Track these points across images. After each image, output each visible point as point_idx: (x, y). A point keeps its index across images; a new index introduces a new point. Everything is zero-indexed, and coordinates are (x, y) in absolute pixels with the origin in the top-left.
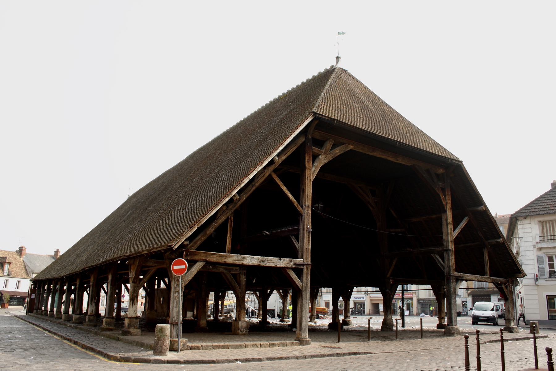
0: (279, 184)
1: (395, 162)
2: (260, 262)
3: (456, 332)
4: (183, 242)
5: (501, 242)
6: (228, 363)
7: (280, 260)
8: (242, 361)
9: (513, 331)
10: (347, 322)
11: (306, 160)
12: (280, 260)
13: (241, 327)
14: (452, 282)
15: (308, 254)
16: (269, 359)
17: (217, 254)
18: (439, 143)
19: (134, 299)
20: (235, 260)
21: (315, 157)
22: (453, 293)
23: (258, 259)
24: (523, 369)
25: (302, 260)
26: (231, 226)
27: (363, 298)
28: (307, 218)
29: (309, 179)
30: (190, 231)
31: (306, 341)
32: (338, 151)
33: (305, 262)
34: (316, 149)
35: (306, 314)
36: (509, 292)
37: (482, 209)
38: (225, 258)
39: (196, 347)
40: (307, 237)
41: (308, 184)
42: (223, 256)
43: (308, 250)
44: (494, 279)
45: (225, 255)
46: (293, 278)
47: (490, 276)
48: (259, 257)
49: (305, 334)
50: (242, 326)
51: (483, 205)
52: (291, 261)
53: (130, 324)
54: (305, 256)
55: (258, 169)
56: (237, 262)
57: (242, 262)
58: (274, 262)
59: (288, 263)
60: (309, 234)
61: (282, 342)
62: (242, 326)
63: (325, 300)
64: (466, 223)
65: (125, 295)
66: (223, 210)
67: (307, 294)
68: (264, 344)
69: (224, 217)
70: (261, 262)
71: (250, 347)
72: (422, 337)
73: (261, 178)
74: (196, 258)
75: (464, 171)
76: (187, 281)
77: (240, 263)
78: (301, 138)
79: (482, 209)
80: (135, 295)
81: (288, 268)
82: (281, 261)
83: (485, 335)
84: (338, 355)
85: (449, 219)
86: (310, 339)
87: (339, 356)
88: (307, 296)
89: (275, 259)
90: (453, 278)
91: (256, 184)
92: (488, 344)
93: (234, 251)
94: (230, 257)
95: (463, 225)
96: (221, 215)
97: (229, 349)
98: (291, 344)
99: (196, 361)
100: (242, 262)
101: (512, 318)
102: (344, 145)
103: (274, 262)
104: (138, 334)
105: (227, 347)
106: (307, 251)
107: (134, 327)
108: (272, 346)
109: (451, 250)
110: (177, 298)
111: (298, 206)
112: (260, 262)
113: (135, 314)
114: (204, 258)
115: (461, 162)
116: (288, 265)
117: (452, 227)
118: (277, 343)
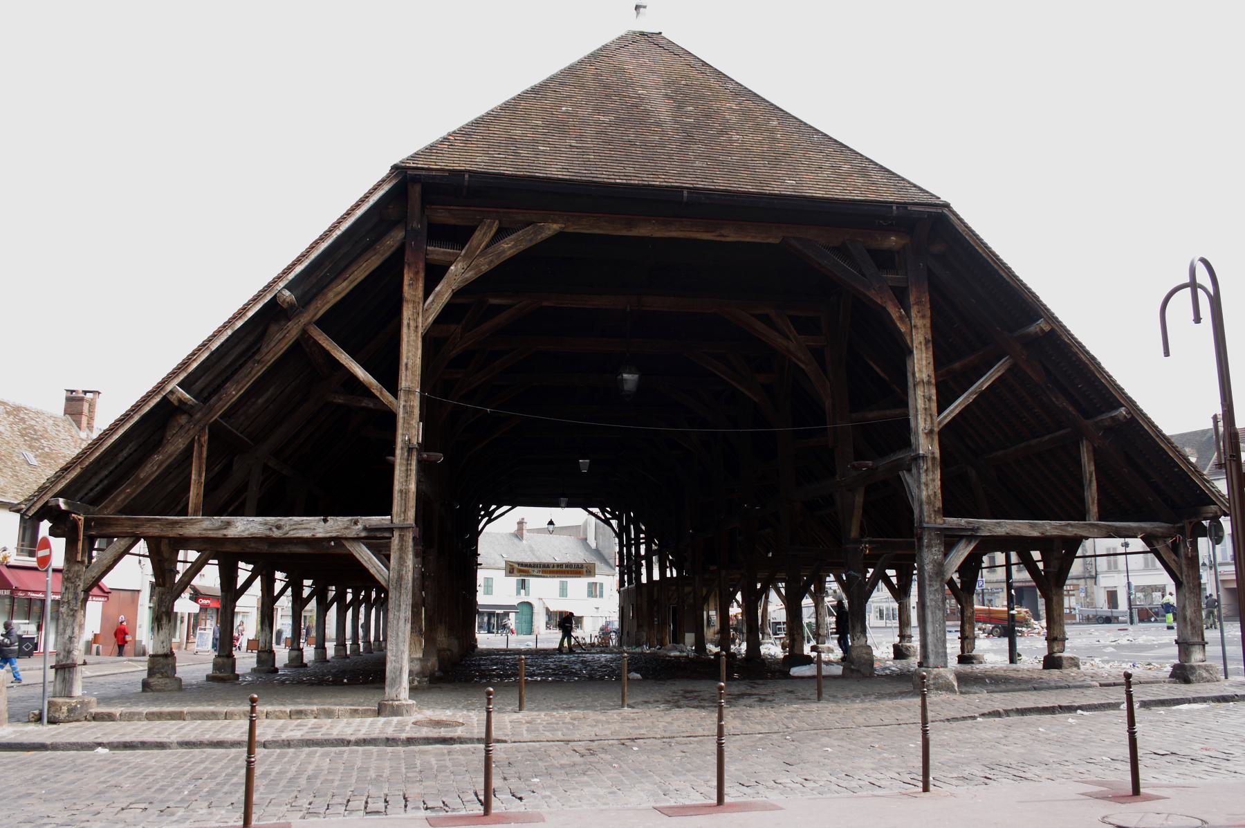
0: (328, 348)
1: (716, 241)
2: (270, 529)
3: (934, 684)
4: (47, 502)
5: (1121, 418)
6: (77, 750)
7: (325, 521)
8: (113, 746)
9: (1191, 678)
10: (902, 650)
11: (406, 282)
12: (325, 521)
14: (930, 546)
15: (405, 504)
16: (186, 745)
17: (162, 519)
18: (884, 166)
19: (162, 619)
20: (205, 530)
21: (434, 274)
22: (930, 576)
23: (266, 524)
24: (225, 825)
25: (389, 517)
26: (200, 457)
28: (404, 418)
29: (412, 324)
30: (64, 477)
31: (392, 706)
32: (508, 247)
33: (394, 521)
34: (437, 252)
35: (397, 645)
36: (1184, 561)
37: (1038, 329)
38: (181, 527)
39: (107, 715)
40: (405, 462)
41: (409, 337)
42: (176, 522)
43: (406, 494)
44: (1117, 527)
45: (180, 520)
46: (361, 560)
47: (1100, 520)
48: (268, 518)
49: (394, 690)
51: (1041, 317)
52: (356, 523)
53: (153, 668)
54: (396, 508)
55: (233, 326)
56: (212, 534)
57: (225, 532)
58: (308, 526)
59: (346, 528)
60: (408, 455)
61: (326, 707)
63: (1105, 587)
64: (999, 374)
66: (178, 424)
67: (400, 596)
68: (275, 711)
69: (180, 440)
70: (274, 529)
71: (237, 717)
72: (819, 698)
73: (277, 343)
74: (112, 531)
75: (960, 228)
76: (90, 579)
77: (220, 534)
78: (392, 234)
79: (1038, 329)
80: (164, 610)
81: (346, 539)
82: (328, 524)
83: (1066, 690)
84: (390, 742)
85: (920, 371)
86: (414, 702)
87: (394, 744)
88: (400, 601)
89: (311, 520)
90: (933, 534)
91: (265, 358)
92: (980, 723)
93: (211, 509)
94: (192, 523)
95: (983, 383)
96: (174, 435)
97: (184, 720)
98: (351, 713)
99: (8, 743)
100: (225, 532)
101: (1196, 640)
103: (307, 528)
104: (166, 689)
105: (214, 716)
106: (404, 495)
107: (162, 674)
108: (298, 717)
109: (924, 457)
110: (65, 615)
112: (270, 529)
114: (130, 531)
115: (947, 206)
116: (348, 531)
117: (934, 391)
118: (312, 711)
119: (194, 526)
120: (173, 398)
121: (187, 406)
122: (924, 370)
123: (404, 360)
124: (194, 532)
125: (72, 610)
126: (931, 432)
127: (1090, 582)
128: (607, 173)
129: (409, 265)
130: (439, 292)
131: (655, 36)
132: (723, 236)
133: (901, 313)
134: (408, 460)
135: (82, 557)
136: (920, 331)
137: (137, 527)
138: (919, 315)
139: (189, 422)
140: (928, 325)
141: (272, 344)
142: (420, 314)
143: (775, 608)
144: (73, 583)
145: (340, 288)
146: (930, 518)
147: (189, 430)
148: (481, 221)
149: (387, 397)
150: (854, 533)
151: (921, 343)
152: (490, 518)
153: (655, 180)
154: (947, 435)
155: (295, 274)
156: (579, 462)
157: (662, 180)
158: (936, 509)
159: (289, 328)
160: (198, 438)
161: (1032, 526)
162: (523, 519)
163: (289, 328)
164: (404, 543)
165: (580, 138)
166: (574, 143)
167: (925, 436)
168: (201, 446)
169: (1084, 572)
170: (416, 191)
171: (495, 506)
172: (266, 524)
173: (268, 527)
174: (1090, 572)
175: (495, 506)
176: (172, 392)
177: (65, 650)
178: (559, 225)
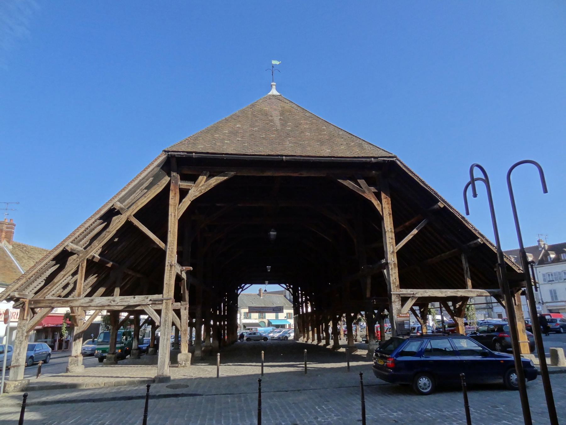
2: (110, 302)
5: (479, 243)
7: (134, 298)
13: (180, 360)
20: (82, 303)
27: (539, 307)
28: (169, 253)
34: (184, 185)
40: (169, 272)
50: (181, 359)
60: (170, 269)
62: (181, 359)
63: (497, 313)
65: (189, 328)
70: (112, 302)
82: (135, 299)
85: (387, 227)
102: (222, 173)
111: (160, 243)
112: (110, 302)
113: (76, 353)
117: (394, 235)
119: (77, 302)
120: (67, 248)
121: (76, 251)
122: (389, 226)
123: (169, 229)
124: (77, 304)
125: (20, 341)
126: (393, 252)
127: (490, 310)
128: (252, 150)
129: (172, 190)
130: (184, 201)
131: (279, 96)
132: (302, 174)
133: (378, 202)
134: (170, 271)
135: (26, 317)
136: (386, 210)
137: (52, 303)
138: (386, 203)
139: (77, 258)
140: (390, 207)
141: (114, 225)
142: (177, 210)
143: (342, 327)
144: (22, 329)
145: (143, 201)
146: (394, 289)
147: (77, 260)
148: (202, 172)
149: (162, 245)
150: (368, 295)
151: (387, 215)
152: (242, 289)
153: (272, 152)
154: (400, 254)
155: (122, 195)
156: (267, 268)
157: (274, 152)
158: (396, 285)
159: (121, 218)
160: (81, 265)
161: (442, 292)
162: (261, 289)
163: (121, 218)
164: (168, 306)
165: (242, 137)
166: (240, 139)
167: (390, 254)
168: (82, 268)
169: (487, 306)
170: (174, 162)
171: (244, 285)
172: (108, 300)
173: (109, 301)
174: (490, 306)
175: (244, 285)
176: (67, 246)
177: (16, 359)
178: (234, 173)
